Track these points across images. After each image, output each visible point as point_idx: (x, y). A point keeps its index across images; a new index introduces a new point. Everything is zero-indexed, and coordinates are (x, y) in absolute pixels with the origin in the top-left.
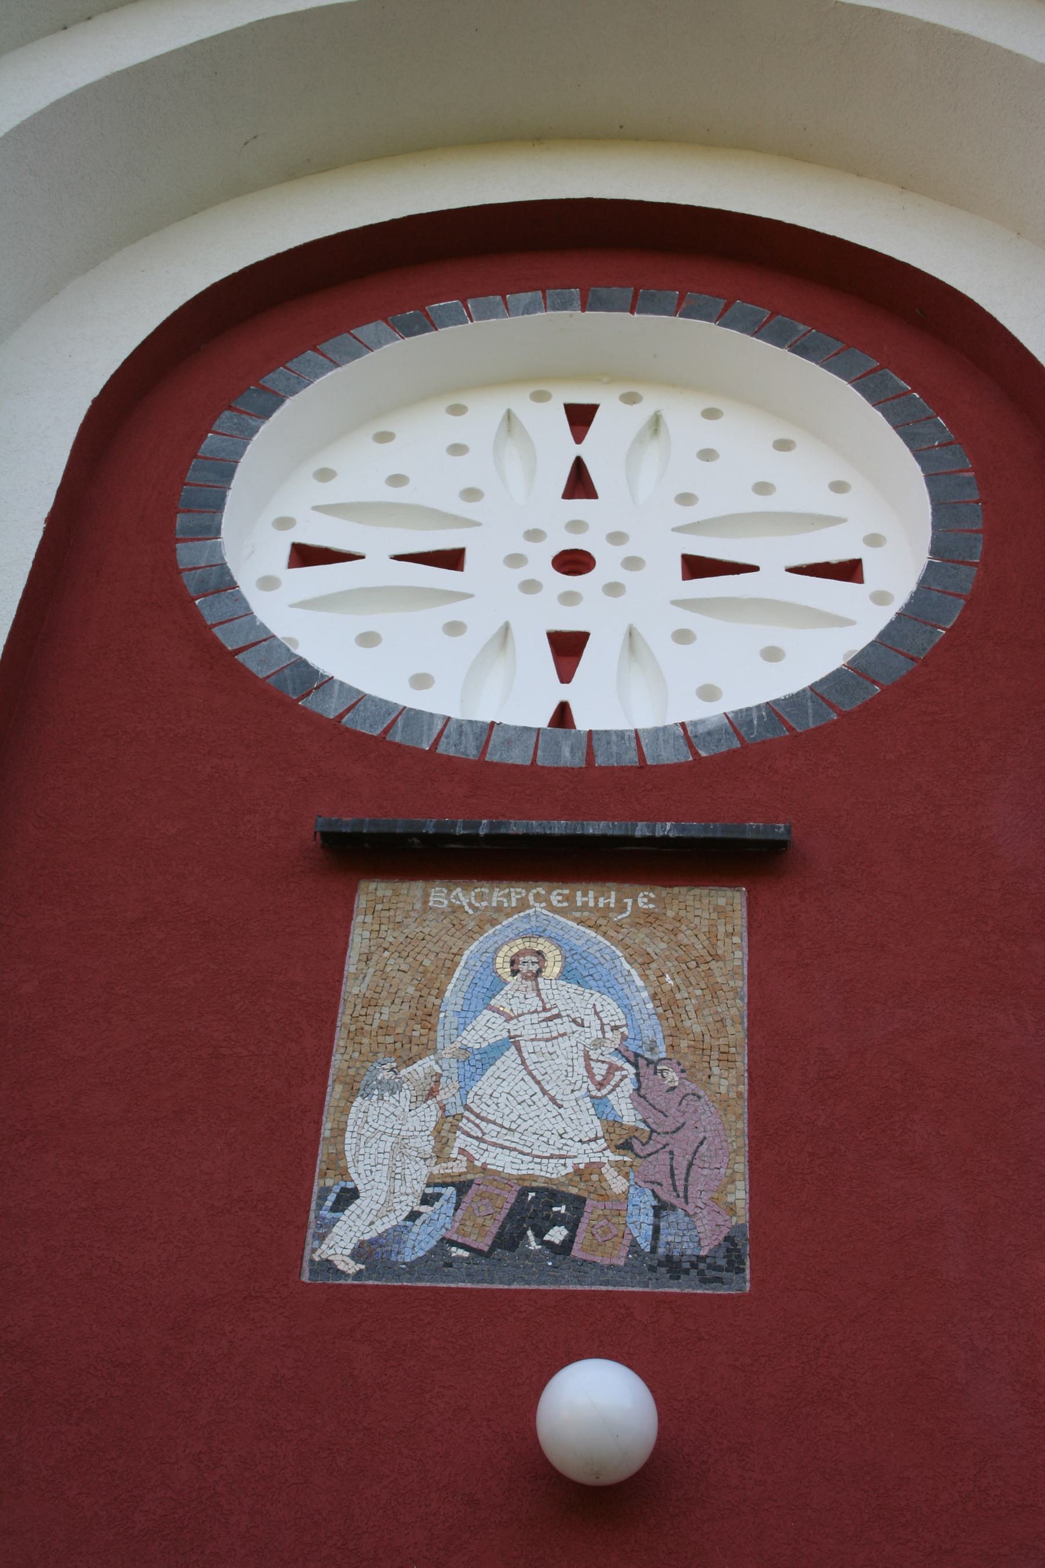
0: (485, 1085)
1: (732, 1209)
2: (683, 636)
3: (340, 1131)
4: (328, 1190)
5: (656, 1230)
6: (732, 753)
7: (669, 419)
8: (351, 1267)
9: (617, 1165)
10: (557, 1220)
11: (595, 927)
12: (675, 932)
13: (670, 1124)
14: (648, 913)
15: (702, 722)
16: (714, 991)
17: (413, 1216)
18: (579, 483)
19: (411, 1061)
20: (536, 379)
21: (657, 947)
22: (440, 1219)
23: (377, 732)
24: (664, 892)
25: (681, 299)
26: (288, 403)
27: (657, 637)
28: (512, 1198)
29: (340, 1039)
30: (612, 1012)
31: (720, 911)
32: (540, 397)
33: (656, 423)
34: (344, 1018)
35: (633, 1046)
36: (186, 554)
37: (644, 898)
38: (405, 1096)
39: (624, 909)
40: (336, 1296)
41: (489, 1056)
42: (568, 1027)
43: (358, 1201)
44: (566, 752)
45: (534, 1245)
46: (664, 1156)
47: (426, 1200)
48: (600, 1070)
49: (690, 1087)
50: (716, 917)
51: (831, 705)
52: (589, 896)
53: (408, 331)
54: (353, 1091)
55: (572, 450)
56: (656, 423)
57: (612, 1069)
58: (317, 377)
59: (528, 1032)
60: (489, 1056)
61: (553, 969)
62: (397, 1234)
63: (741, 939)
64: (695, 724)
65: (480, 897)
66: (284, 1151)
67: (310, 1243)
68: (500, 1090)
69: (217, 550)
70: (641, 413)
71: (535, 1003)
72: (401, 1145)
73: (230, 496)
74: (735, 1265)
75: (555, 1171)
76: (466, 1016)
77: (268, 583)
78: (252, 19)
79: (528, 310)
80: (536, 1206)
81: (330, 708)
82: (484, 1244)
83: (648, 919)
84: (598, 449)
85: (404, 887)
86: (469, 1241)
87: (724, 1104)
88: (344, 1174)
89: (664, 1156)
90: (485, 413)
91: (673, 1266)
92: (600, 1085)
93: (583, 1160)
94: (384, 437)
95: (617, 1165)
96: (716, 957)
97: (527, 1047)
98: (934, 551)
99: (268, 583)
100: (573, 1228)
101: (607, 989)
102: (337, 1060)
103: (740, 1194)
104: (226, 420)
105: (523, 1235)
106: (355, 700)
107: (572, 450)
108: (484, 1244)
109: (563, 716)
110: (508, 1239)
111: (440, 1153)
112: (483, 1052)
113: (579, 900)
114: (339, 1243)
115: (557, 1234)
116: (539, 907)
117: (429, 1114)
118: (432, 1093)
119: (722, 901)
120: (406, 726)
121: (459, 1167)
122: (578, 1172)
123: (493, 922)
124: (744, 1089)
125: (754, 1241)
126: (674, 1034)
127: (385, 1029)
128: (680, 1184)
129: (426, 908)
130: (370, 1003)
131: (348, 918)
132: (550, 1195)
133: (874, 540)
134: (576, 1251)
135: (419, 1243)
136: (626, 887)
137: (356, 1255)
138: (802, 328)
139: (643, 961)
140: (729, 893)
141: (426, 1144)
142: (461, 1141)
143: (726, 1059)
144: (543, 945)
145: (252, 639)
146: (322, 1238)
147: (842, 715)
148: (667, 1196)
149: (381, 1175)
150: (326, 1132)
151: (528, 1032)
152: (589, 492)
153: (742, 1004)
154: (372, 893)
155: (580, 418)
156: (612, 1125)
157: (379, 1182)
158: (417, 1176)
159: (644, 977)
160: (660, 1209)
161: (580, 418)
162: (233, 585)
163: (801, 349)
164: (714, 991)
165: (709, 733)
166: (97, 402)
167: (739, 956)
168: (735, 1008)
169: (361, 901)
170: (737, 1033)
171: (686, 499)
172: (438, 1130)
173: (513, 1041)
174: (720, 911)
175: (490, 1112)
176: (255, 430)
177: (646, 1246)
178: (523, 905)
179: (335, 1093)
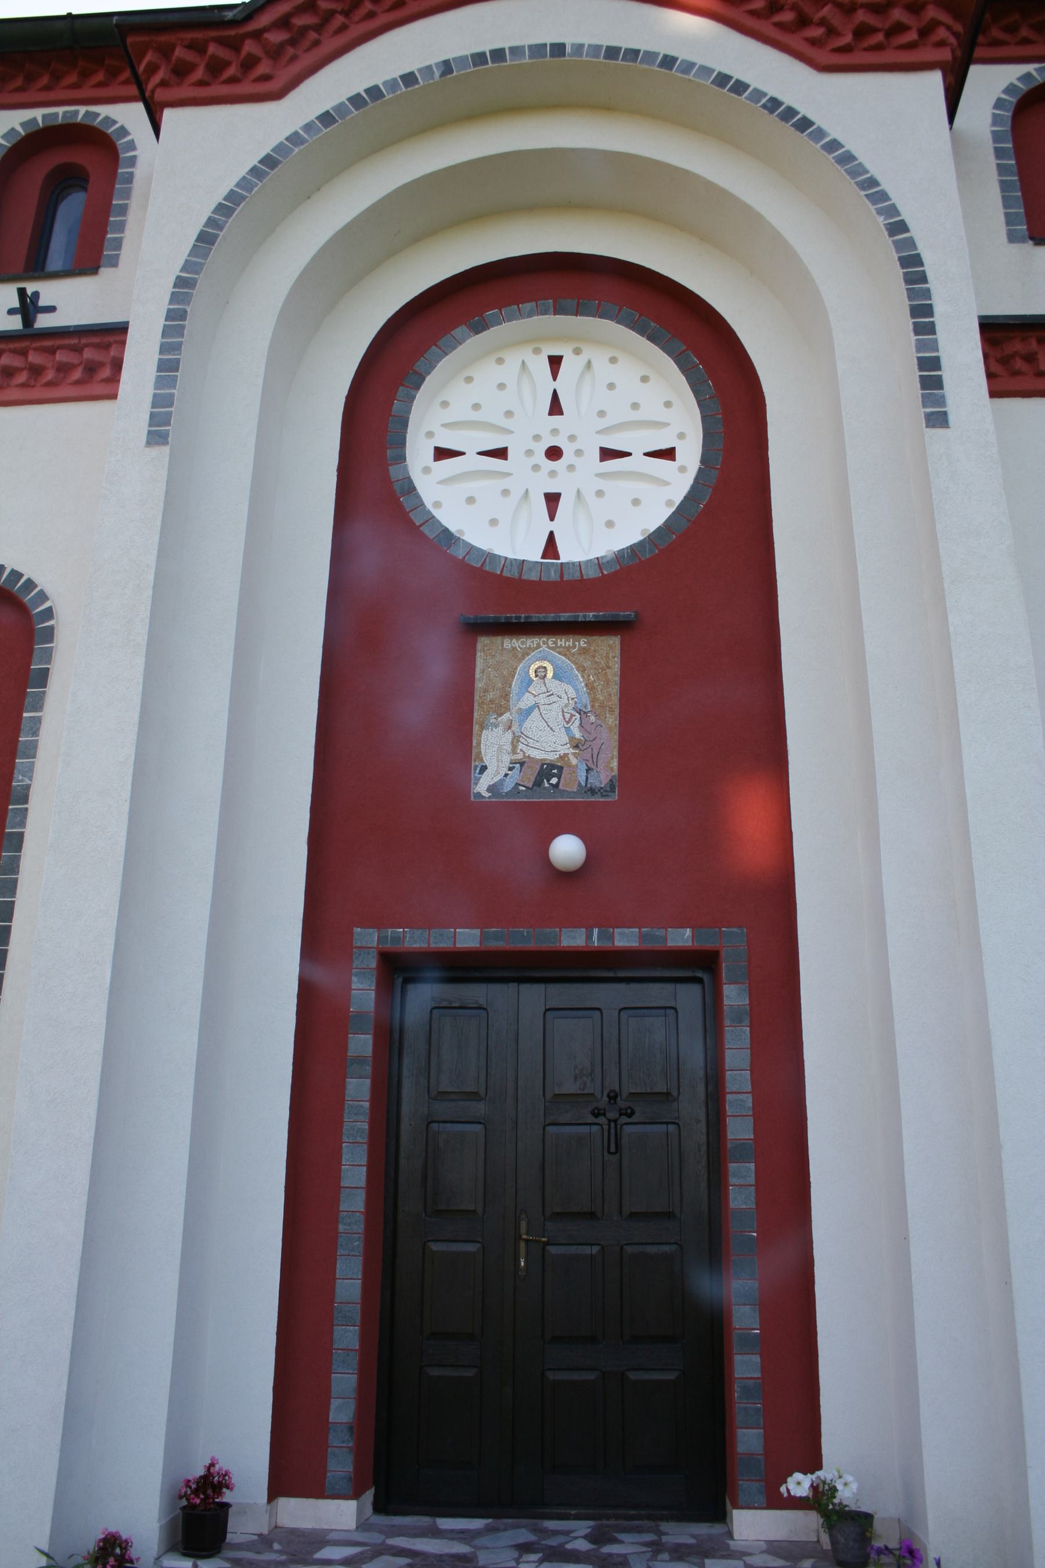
0: (527, 724)
1: (612, 769)
2: (600, 493)
3: (479, 744)
4: (476, 767)
5: (587, 778)
6: (616, 572)
7: (595, 365)
8: (487, 795)
9: (574, 754)
10: (554, 775)
11: (565, 655)
12: (594, 657)
13: (591, 737)
14: (584, 648)
15: (605, 557)
16: (608, 682)
17: (506, 775)
18: (556, 408)
19: (501, 715)
20: (534, 341)
21: (587, 664)
22: (515, 776)
23: (479, 565)
24: (590, 638)
25: (599, 306)
26: (428, 379)
27: (589, 495)
28: (538, 767)
29: (476, 707)
30: (572, 693)
31: (611, 647)
33: (589, 364)
34: (477, 698)
35: (579, 706)
36: (394, 472)
37: (583, 642)
38: (501, 728)
39: (574, 647)
40: (482, 807)
41: (529, 711)
42: (556, 699)
44: (553, 573)
45: (547, 785)
46: (589, 750)
47: (510, 769)
48: (567, 716)
49: (599, 722)
50: (609, 647)
51: (656, 546)
52: (563, 642)
53: (478, 329)
54: (482, 727)
55: (552, 385)
56: (589, 364)
57: (572, 716)
58: (438, 362)
59: (542, 701)
60: (529, 711)
61: (550, 674)
62: (501, 782)
63: (617, 660)
64: (602, 557)
65: (523, 643)
67: (473, 786)
68: (533, 725)
69: (406, 468)
70: (581, 361)
71: (544, 689)
72: (500, 748)
73: (408, 436)
74: (612, 790)
75: (552, 757)
76: (520, 695)
77: (427, 470)
78: (394, 187)
79: (530, 315)
80: (548, 770)
81: (460, 554)
82: (530, 785)
83: (583, 651)
85: (494, 639)
86: (525, 784)
87: (610, 729)
88: (482, 760)
89: (589, 750)
90: (513, 359)
91: (592, 791)
92: (568, 723)
93: (562, 753)
94: (469, 380)
95: (574, 754)
96: (609, 667)
97: (542, 707)
98: (702, 462)
99: (427, 470)
100: (559, 778)
101: (569, 683)
102: (476, 715)
103: (615, 764)
104: (401, 391)
105: (543, 781)
107: (552, 385)
108: (530, 785)
109: (551, 548)
110: (538, 783)
111: (514, 750)
112: (526, 710)
113: (559, 643)
114: (482, 786)
115: (554, 781)
116: (544, 647)
117: (509, 736)
118: (510, 727)
119: (611, 642)
120: (490, 562)
121: (520, 756)
122: (561, 757)
123: (528, 655)
124: (617, 722)
125: (619, 781)
126: (593, 700)
127: (492, 701)
128: (595, 757)
129: (503, 649)
130: (486, 691)
131: (475, 654)
132: (552, 766)
133: (681, 436)
134: (561, 787)
136: (577, 637)
137: (488, 790)
138: (653, 324)
139: (582, 669)
140: (614, 638)
141: (509, 748)
142: (521, 746)
143: (611, 711)
144: (546, 664)
145: (426, 518)
146: (476, 784)
147: (660, 550)
148: (591, 765)
149: (494, 760)
150: (474, 744)
151: (542, 701)
152: (561, 413)
153: (617, 687)
154: (484, 642)
155: (555, 362)
156: (572, 738)
157: (496, 761)
158: (507, 759)
159: (583, 677)
160: (588, 770)
161: (555, 362)
162: (414, 489)
163: (652, 339)
164: (608, 682)
165: (608, 562)
166: (347, 398)
167: (617, 667)
168: (615, 689)
169: (479, 646)
170: (615, 699)
171: (602, 414)
172: (512, 742)
173: (537, 706)
174: (611, 647)
175: (530, 734)
176: (414, 397)
177: (583, 784)
178: (539, 646)
179: (476, 728)
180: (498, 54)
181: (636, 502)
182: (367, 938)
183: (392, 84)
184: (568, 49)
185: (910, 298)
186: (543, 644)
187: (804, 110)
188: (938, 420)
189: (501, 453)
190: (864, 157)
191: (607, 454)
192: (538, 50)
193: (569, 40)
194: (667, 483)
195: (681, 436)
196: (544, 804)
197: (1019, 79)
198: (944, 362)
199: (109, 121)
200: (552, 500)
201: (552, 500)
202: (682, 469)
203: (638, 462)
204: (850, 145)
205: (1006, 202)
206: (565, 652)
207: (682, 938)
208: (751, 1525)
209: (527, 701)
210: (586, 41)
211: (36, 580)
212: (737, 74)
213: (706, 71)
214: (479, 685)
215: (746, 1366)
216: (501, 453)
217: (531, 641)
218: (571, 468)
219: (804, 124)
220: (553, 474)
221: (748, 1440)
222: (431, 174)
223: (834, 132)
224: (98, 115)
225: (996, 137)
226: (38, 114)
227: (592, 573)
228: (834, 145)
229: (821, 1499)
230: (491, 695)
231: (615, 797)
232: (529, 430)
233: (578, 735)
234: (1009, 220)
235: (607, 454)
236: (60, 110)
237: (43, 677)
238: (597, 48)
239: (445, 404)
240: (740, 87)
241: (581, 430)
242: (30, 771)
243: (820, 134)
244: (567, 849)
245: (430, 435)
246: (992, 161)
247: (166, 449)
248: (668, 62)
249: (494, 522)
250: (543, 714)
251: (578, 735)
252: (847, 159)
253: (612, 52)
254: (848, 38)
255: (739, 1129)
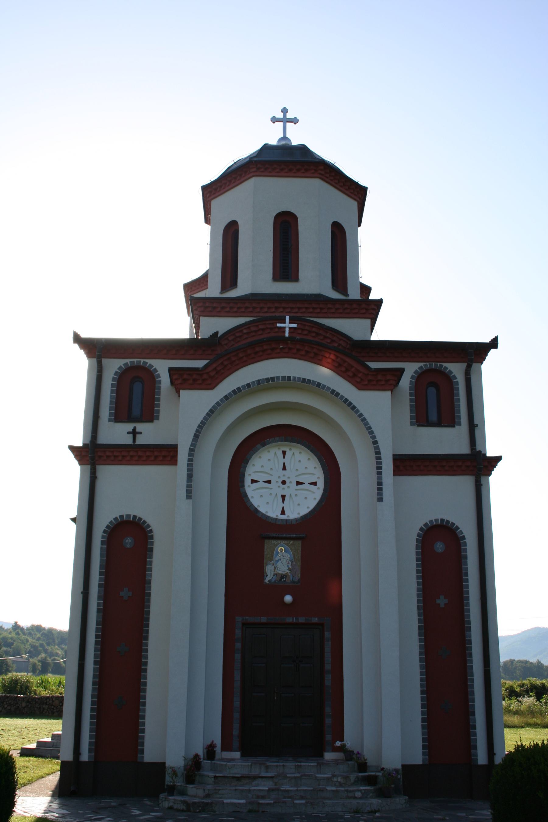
0: (278, 564)
18: (284, 468)
27: (293, 496)
30: (289, 556)
32: (279, 449)
41: (278, 561)
43: (309, 765)
50: (299, 543)
60: (278, 561)
62: (271, 580)
66: (262, 573)
68: (279, 564)
75: (284, 573)
77: (249, 486)
80: (283, 576)
84: (287, 460)
91: (294, 582)
106: (257, 491)
110: (281, 580)
111: (274, 571)
114: (267, 580)
117: (273, 567)
132: (284, 575)
135: (273, 581)
139: (292, 550)
141: (273, 570)
152: (286, 470)
154: (266, 541)
155: (284, 453)
156: (289, 568)
157: (269, 573)
158: (273, 573)
161: (284, 453)
167: (300, 549)
168: (300, 555)
170: (300, 558)
180: (273, 379)
181: (306, 498)
182: (239, 619)
183: (243, 386)
184: (292, 378)
185: (377, 464)
186: (282, 542)
187: (354, 403)
188: (380, 500)
189: (269, 482)
190: (369, 420)
191: (298, 483)
192: (283, 378)
193: (292, 375)
194: (314, 493)
195: (318, 478)
196: (282, 585)
197: (419, 368)
198: (384, 484)
199: (151, 366)
200: (283, 497)
201: (283, 497)
202: (318, 488)
203: (306, 486)
204: (366, 415)
205: (411, 411)
206: (287, 545)
207: (315, 620)
208: (329, 756)
209: (278, 558)
210: (297, 376)
211: (147, 520)
212: (337, 390)
213: (329, 388)
214: (265, 553)
215: (328, 721)
216: (269, 482)
217: (279, 541)
218: (288, 487)
219: (354, 408)
220: (283, 489)
221: (328, 737)
222: (254, 408)
223: (362, 411)
224: (147, 363)
225: (410, 389)
226: (128, 361)
227: (294, 523)
228: (361, 415)
229: (342, 749)
230: (268, 556)
231: (300, 584)
232: (277, 475)
233: (290, 567)
234: (411, 418)
235: (298, 483)
236: (135, 360)
237: (151, 550)
238: (299, 378)
239: (254, 465)
240: (337, 394)
241: (291, 476)
242: (151, 575)
243: (357, 411)
244: (288, 598)
245: (250, 475)
246: (408, 397)
247: (191, 500)
248: (319, 385)
249: (268, 503)
250: (281, 561)
251: (290, 567)
252: (364, 420)
253: (304, 380)
254: (366, 383)
255: (328, 666)
